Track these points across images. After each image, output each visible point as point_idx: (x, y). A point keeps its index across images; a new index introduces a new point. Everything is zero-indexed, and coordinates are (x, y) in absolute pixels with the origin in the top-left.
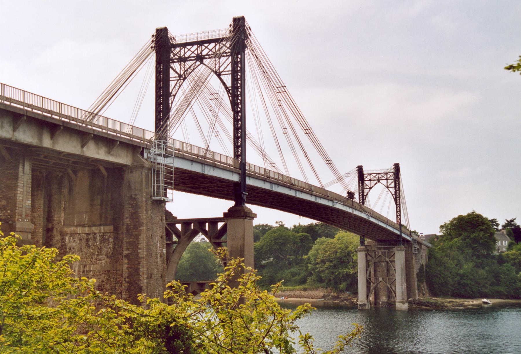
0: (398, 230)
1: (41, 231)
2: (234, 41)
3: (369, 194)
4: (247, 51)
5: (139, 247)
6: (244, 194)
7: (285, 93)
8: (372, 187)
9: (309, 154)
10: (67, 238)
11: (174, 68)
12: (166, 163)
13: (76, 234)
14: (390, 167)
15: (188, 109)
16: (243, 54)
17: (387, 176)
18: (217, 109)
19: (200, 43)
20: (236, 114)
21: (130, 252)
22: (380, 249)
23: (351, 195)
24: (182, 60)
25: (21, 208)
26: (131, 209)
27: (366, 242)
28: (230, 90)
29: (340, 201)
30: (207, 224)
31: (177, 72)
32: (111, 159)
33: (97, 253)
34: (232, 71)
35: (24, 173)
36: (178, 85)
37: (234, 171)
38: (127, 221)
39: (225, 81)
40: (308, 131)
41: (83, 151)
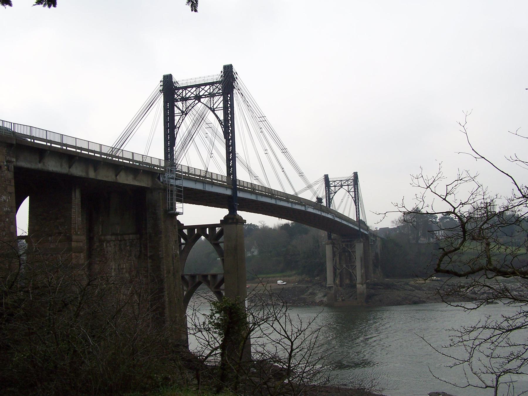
0: (358, 227)
2: (224, 85)
3: (334, 197)
4: (235, 91)
5: (159, 250)
6: (236, 205)
7: (265, 122)
8: (337, 192)
9: (285, 169)
11: (177, 106)
12: (176, 184)
13: (111, 241)
14: (351, 175)
15: (191, 141)
16: (232, 93)
17: (348, 182)
18: (214, 138)
19: (198, 86)
20: (227, 141)
22: (344, 242)
23: (319, 200)
24: (184, 99)
27: (332, 237)
28: (222, 122)
29: (311, 206)
30: (208, 229)
31: (179, 109)
32: (136, 183)
33: (128, 255)
34: (223, 107)
35: (75, 198)
36: (181, 119)
37: (228, 187)
39: (217, 114)
40: (284, 151)
41: (116, 179)
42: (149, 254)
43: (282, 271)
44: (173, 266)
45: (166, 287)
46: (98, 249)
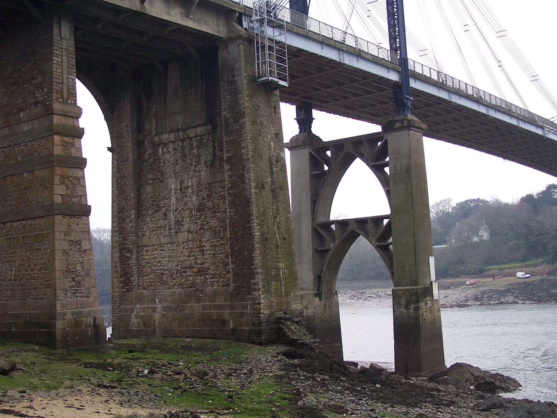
1: (130, 144)
9: (503, 63)
10: (160, 150)
13: (170, 142)
21: (231, 154)
25: (59, 83)
26: (229, 97)
33: (194, 163)
38: (225, 114)
42: (225, 156)
43: (524, 259)
44: (272, 177)
45: (254, 212)
46: (151, 160)
